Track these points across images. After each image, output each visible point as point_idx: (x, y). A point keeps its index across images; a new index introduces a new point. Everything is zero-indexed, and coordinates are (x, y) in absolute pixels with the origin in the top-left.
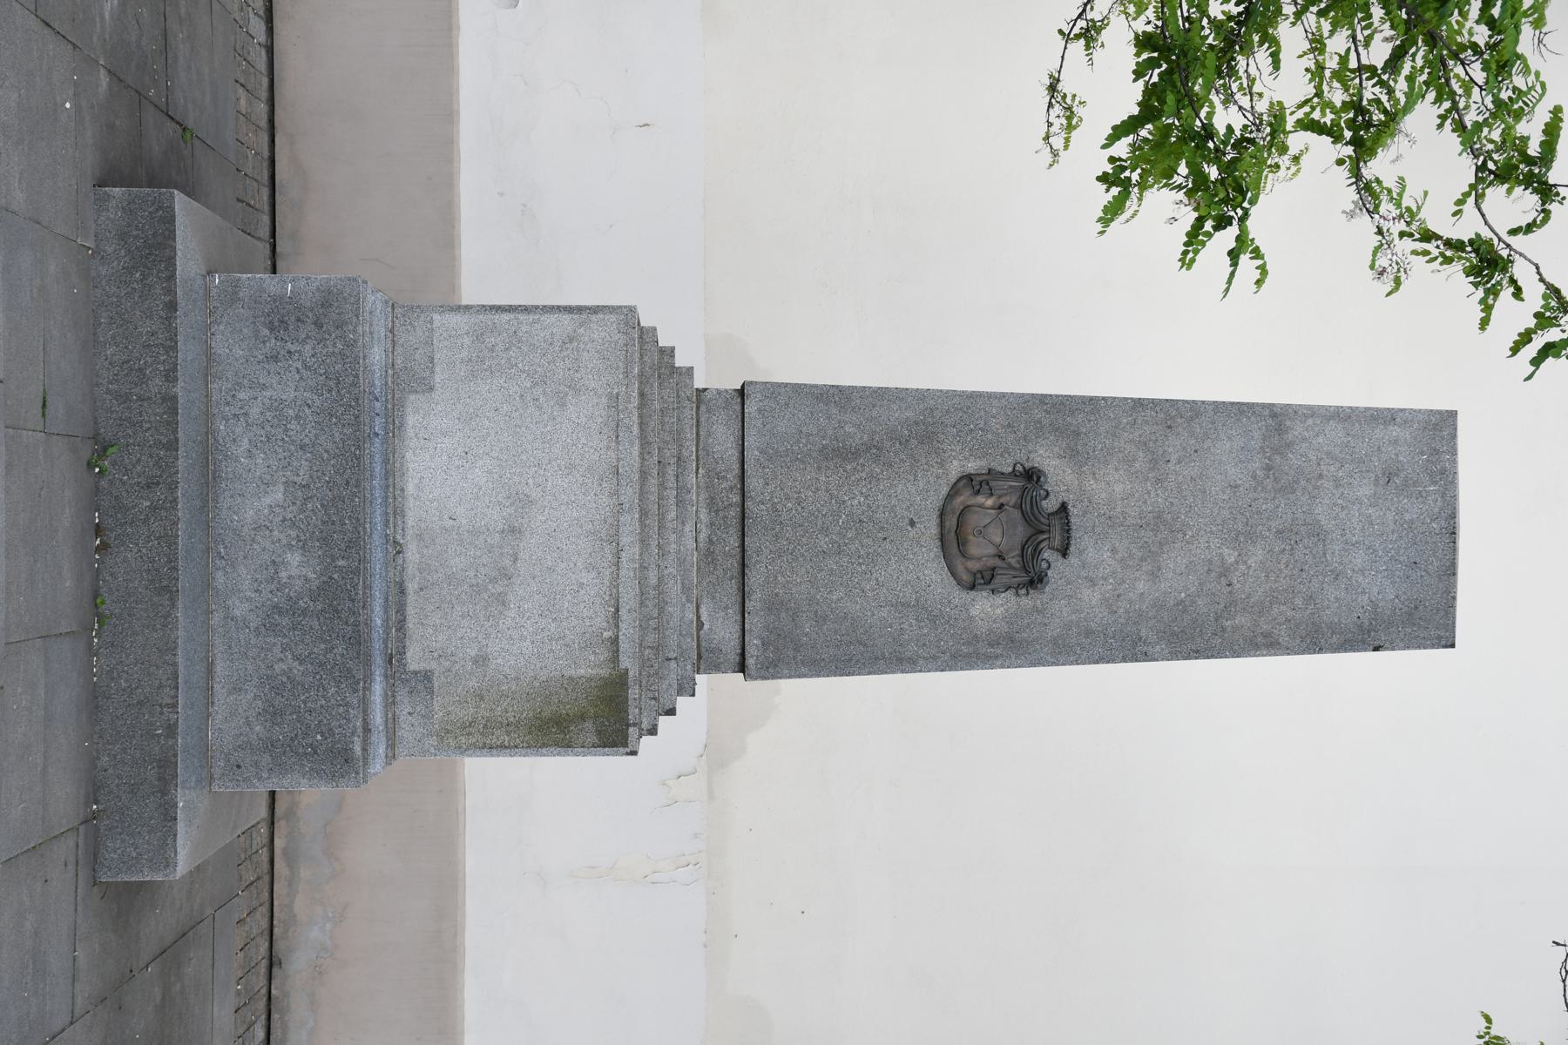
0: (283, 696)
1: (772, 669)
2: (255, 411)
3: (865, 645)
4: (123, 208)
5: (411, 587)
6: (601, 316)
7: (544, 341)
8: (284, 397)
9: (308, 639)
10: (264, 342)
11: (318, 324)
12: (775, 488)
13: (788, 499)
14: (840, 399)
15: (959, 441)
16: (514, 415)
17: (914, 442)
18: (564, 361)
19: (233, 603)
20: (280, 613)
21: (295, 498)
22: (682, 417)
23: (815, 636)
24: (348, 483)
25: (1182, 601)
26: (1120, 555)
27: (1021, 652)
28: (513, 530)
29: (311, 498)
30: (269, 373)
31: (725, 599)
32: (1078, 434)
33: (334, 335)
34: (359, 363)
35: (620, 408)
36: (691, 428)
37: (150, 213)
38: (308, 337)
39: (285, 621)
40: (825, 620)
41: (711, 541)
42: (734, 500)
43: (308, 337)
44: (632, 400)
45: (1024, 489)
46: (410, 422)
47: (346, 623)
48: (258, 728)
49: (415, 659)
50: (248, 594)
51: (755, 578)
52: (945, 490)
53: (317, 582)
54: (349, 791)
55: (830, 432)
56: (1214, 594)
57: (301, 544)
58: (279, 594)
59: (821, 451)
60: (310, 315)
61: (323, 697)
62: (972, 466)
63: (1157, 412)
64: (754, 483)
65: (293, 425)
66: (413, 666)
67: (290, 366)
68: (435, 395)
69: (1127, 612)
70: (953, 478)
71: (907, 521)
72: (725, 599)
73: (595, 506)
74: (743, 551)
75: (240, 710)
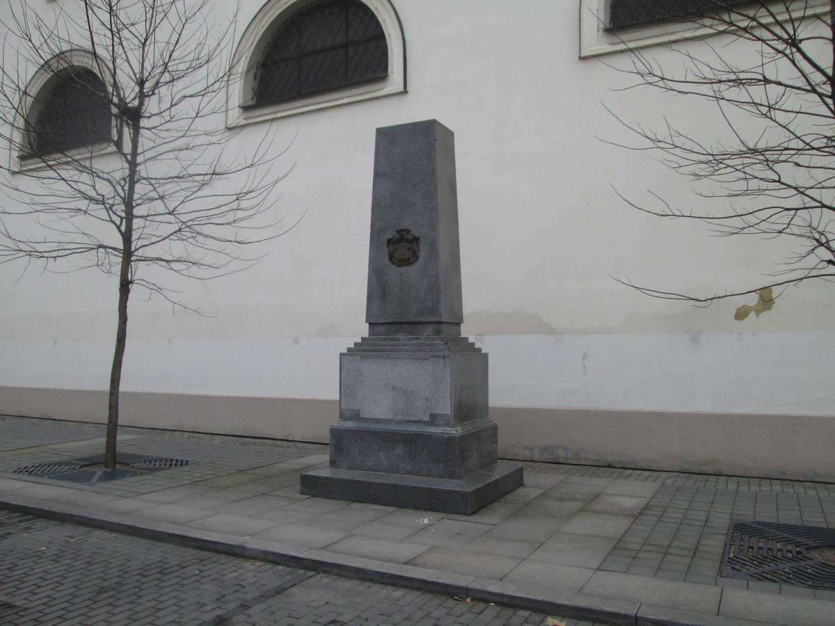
5: (408, 419)
28: (393, 389)
45: (393, 243)
49: (427, 418)
51: (415, 319)
62: (387, 258)
64: (391, 320)
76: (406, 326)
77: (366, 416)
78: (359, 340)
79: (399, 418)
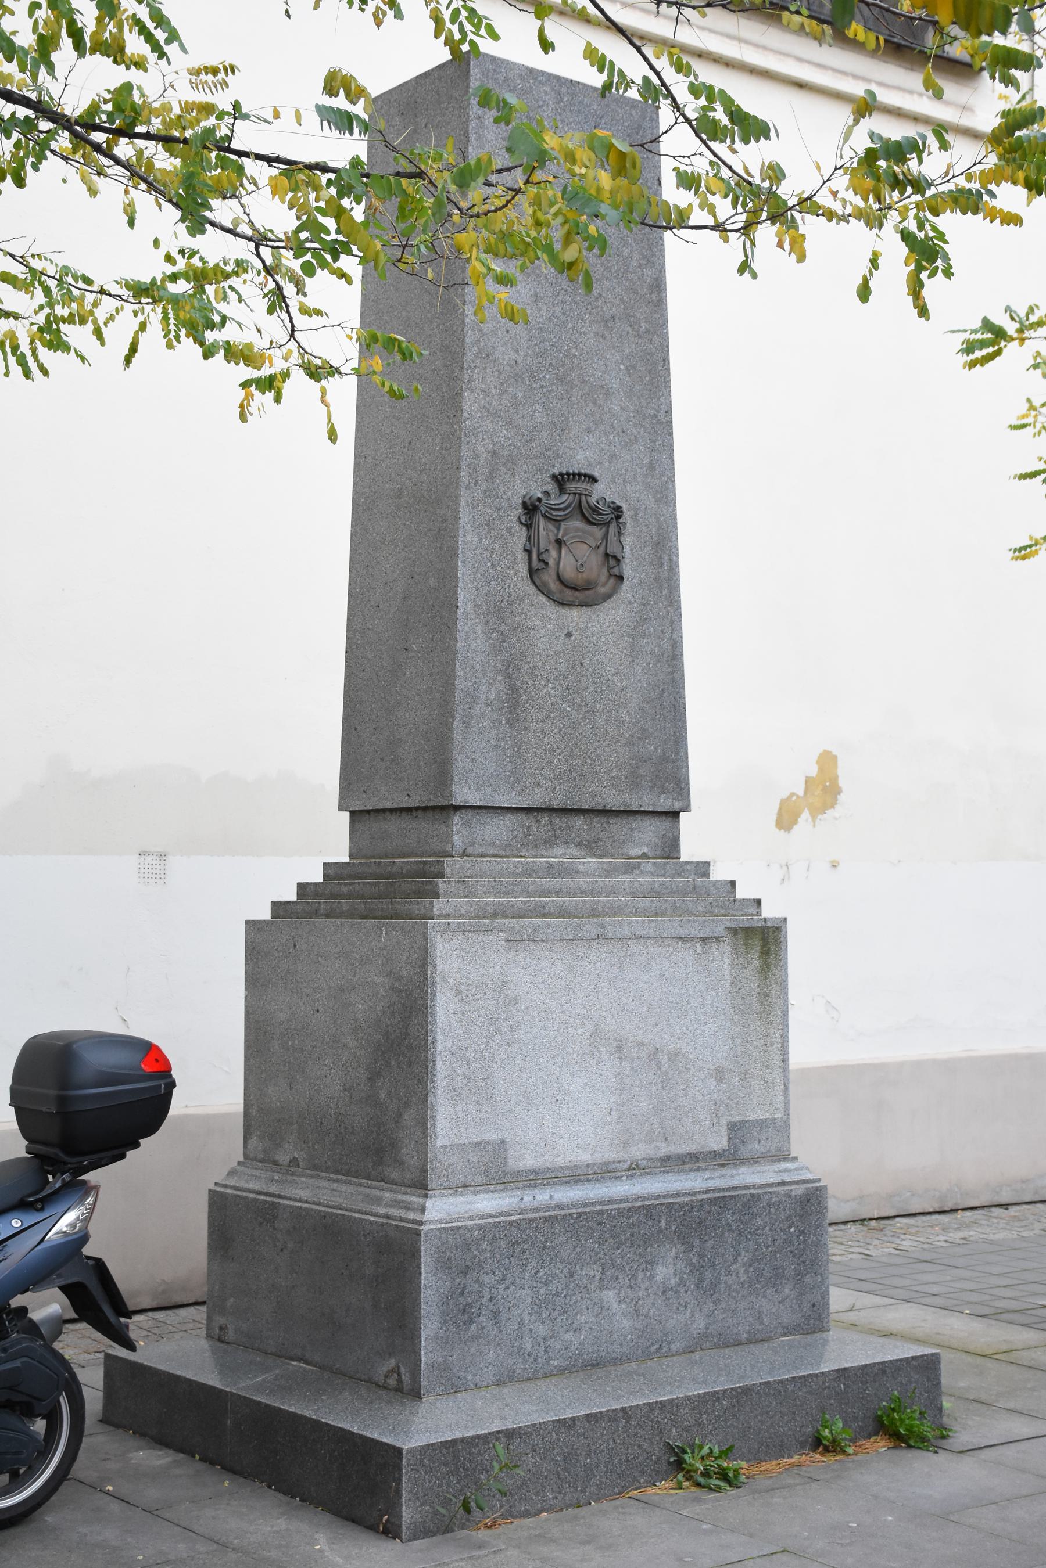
0: (764, 1269)
1: (680, 786)
2: (542, 1330)
3: (663, 691)
4: (422, 1505)
5: (664, 1150)
6: (438, 959)
7: (461, 1021)
8: (530, 1300)
9: (721, 1250)
10: (483, 1328)
11: (465, 1271)
12: (542, 775)
13: (551, 762)
14: (467, 703)
15: (502, 580)
16: (524, 1052)
17: (503, 627)
18: (478, 1000)
19: (695, 1330)
20: (702, 1281)
21: (612, 1277)
22: (488, 873)
23: (657, 740)
24: (600, 1224)
25: (627, 369)
26: (591, 425)
27: (666, 536)
28: (619, 1048)
29: (612, 1261)
30: (510, 1319)
31: (625, 830)
32: (494, 452)
33: (476, 1253)
34: (500, 1223)
35: (518, 938)
36: (498, 863)
37: (426, 1473)
38: (477, 1281)
39: (708, 1275)
40: (645, 730)
41: (579, 844)
42: (547, 819)
43: (477, 1281)
44: (512, 925)
46: (531, 1163)
47: (709, 1212)
48: (787, 1290)
49: (719, 1142)
50: (688, 1315)
51: (613, 800)
52: (542, 598)
53: (678, 1246)
54: (830, 1191)
55: (496, 716)
56: (621, 336)
57: (649, 1267)
58: (688, 1284)
59: (511, 726)
60: (458, 1280)
61: (763, 1229)
62: (523, 570)
63: (475, 367)
64: (538, 798)
65: (552, 1287)
66: (725, 1143)
67: (503, 1298)
68: (508, 1137)
69: (635, 426)
70: (532, 589)
71: (567, 640)
72: (625, 830)
73: (599, 963)
74: (551, 810)
75: (774, 1310)
76: (579, 822)
77: (529, 1162)
78: (316, 876)
79: (639, 1152)
